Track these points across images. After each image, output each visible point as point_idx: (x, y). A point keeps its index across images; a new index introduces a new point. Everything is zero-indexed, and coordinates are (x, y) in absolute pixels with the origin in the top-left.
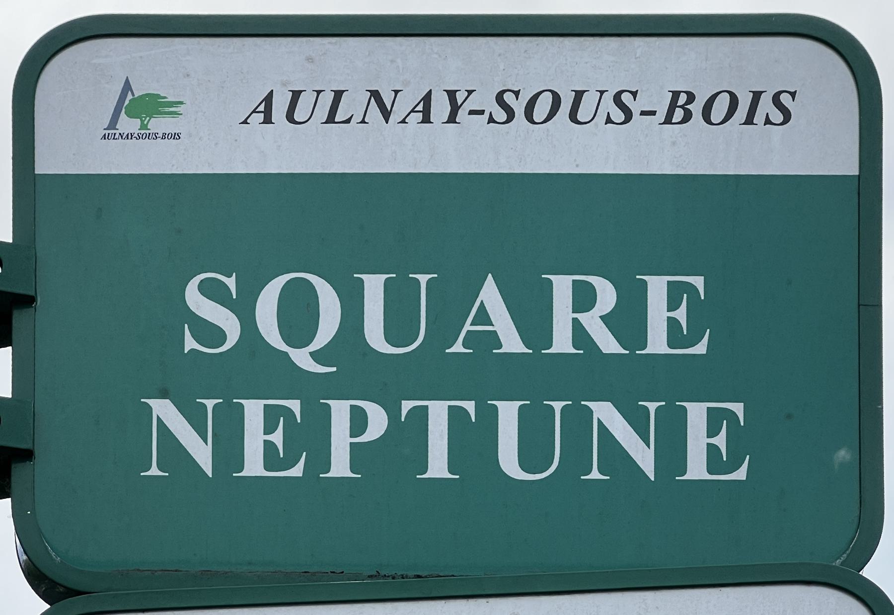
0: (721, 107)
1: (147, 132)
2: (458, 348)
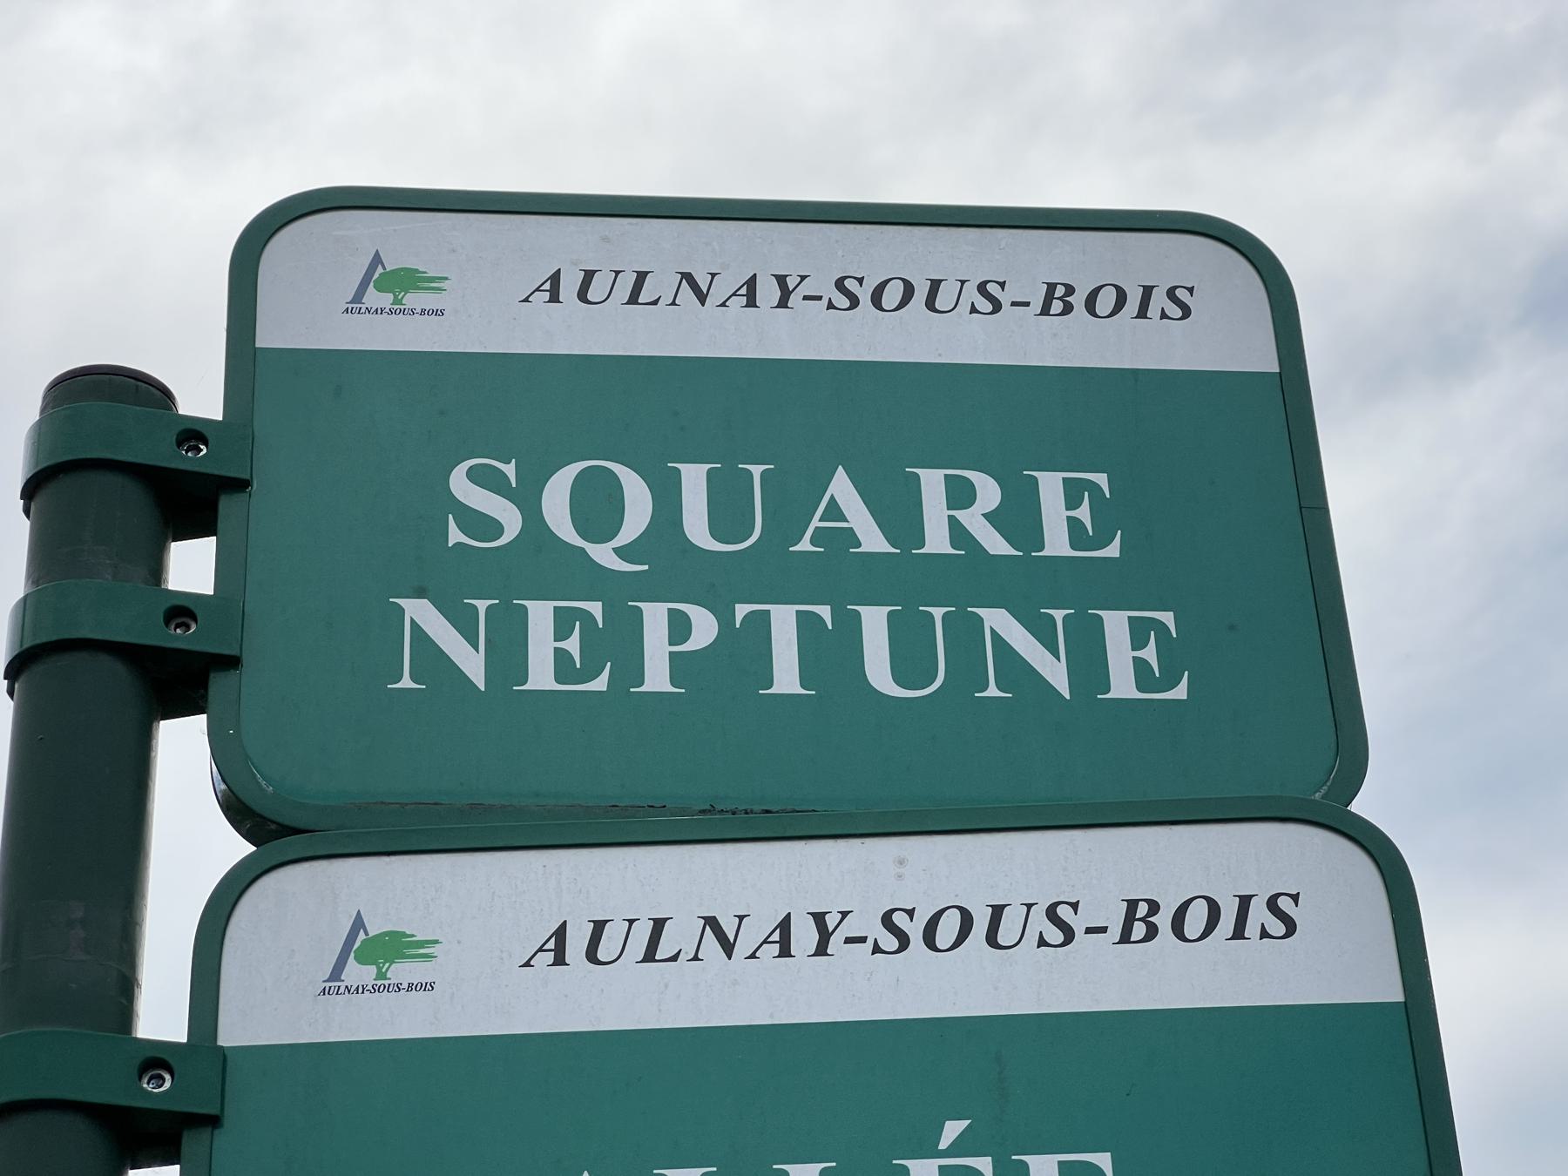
0: (1196, 919)
1: (386, 982)
2: (805, 545)
